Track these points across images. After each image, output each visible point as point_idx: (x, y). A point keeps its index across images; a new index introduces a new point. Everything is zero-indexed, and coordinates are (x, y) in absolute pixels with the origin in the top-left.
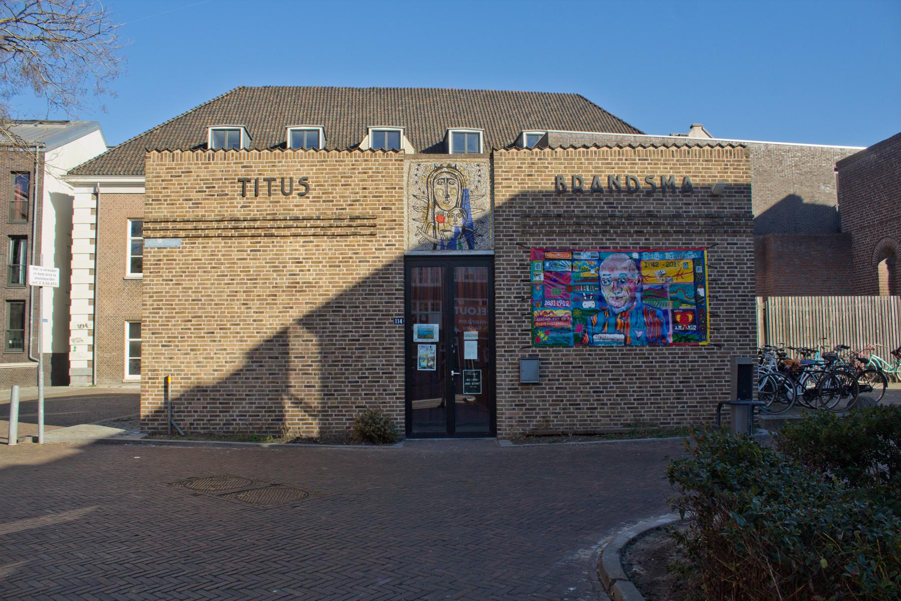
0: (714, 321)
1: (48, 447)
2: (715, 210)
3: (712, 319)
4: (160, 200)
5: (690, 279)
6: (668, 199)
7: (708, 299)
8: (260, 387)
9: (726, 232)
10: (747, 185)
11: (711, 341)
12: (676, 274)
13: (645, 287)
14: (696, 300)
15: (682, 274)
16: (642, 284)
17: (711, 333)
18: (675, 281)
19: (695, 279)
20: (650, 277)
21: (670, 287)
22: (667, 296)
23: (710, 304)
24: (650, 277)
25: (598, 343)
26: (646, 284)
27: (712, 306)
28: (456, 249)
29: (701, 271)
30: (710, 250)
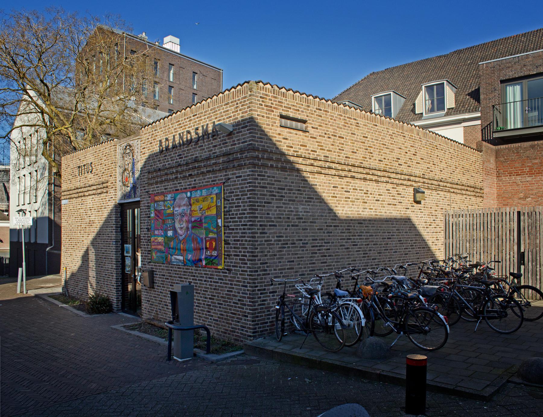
0: (227, 248)
1: (132, 255)
2: (230, 147)
3: (225, 246)
4: (268, 245)
5: (214, 211)
6: (205, 144)
7: (223, 228)
8: (232, 207)
9: (234, 167)
10: (249, 118)
11: (225, 265)
12: (206, 208)
13: (193, 219)
14: (217, 230)
15: (210, 208)
16: (191, 217)
17: (225, 258)
18: (207, 214)
19: (217, 211)
20: (195, 211)
21: (205, 218)
22: (202, 226)
23: (225, 233)
24: (195, 211)
25: (174, 262)
26: (193, 217)
27: (226, 235)
28: (132, 198)
29: (219, 204)
30: (226, 184)
